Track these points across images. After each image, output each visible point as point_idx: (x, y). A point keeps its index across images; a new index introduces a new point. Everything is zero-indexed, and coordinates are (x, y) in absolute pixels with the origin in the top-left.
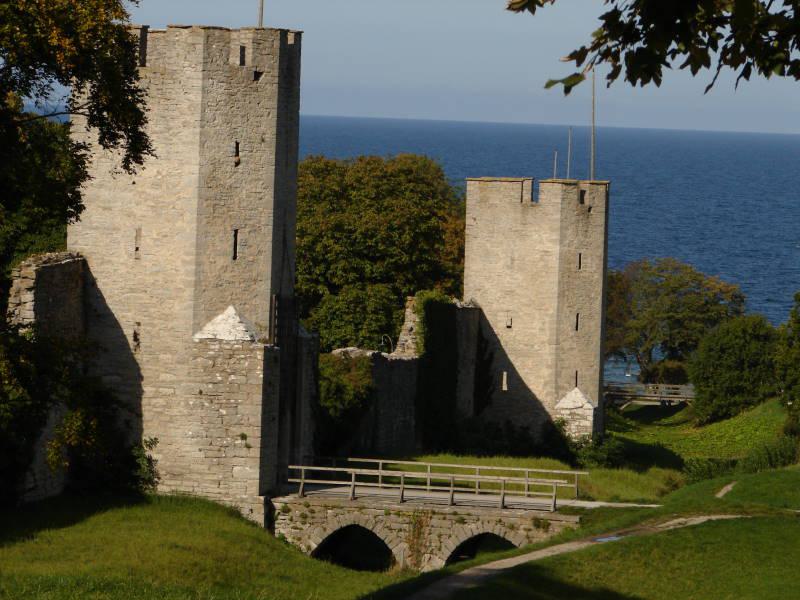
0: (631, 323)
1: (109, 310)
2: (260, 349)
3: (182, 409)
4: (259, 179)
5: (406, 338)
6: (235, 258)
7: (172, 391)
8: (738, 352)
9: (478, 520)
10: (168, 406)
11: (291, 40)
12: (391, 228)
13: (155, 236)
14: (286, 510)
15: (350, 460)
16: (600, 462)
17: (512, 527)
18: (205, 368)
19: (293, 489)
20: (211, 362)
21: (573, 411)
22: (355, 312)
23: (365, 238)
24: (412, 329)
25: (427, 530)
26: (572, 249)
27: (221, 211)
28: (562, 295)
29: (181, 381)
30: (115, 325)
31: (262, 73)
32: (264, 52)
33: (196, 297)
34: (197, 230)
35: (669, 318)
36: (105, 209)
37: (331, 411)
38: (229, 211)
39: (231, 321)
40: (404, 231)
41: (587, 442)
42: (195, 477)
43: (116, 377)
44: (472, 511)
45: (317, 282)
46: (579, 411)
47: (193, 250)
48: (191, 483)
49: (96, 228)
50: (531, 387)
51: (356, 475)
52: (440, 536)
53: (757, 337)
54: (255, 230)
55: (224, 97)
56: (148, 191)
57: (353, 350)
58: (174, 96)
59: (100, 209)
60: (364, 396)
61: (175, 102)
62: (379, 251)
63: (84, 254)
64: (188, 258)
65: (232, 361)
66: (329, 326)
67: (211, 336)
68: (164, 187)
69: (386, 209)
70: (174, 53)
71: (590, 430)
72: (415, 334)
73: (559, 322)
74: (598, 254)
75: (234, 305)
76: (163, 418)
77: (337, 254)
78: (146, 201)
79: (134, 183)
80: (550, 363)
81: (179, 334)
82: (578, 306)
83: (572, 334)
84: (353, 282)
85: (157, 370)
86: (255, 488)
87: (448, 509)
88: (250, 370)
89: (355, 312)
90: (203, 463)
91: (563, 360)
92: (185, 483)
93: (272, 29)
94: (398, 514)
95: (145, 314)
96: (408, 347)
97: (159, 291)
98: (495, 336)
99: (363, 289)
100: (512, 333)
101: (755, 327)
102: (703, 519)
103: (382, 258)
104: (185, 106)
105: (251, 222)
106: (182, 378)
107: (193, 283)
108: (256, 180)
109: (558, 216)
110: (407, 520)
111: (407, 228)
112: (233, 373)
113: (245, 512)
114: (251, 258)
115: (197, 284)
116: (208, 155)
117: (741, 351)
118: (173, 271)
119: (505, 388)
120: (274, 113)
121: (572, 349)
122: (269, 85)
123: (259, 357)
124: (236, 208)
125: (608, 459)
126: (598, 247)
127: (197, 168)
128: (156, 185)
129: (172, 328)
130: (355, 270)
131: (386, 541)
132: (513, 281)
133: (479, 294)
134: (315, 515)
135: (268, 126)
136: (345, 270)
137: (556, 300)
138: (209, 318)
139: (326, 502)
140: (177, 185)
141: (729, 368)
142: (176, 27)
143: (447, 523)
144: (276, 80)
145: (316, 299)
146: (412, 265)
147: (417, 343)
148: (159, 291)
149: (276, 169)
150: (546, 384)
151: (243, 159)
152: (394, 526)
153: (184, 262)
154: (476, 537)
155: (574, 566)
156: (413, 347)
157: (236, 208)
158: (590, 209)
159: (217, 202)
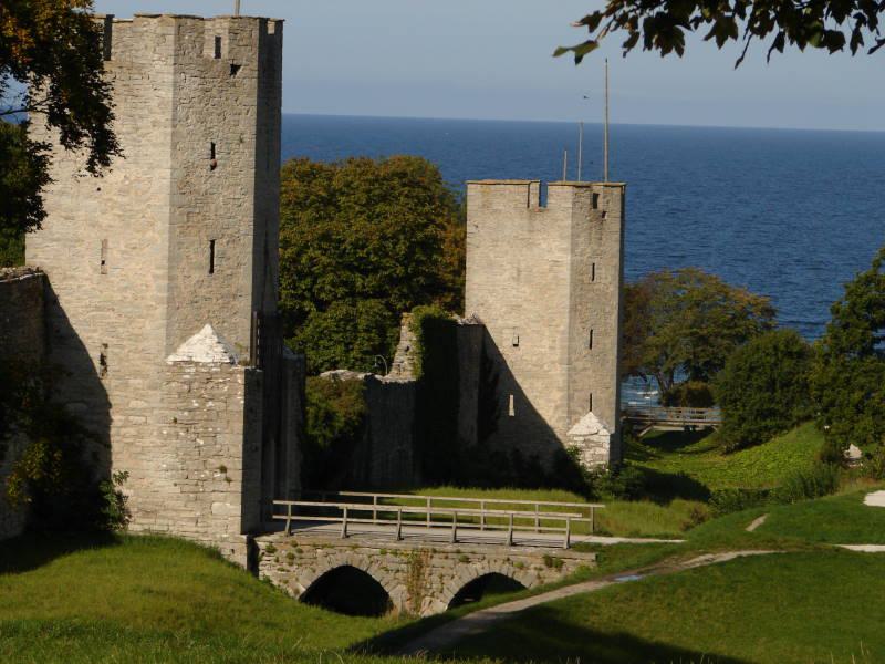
0: (651, 339)
2: (240, 372)
6: (212, 271)
7: (143, 419)
8: (768, 371)
9: (484, 558)
10: (139, 436)
11: (271, 30)
12: (384, 238)
13: (123, 248)
14: (271, 550)
15: (341, 493)
16: (618, 494)
17: (522, 567)
18: (180, 394)
19: (278, 526)
20: (186, 387)
22: (345, 331)
24: (408, 349)
28: (573, 309)
30: (80, 347)
31: (239, 67)
32: (241, 43)
33: (169, 316)
35: (692, 334)
36: (67, 218)
39: (208, 341)
40: (399, 240)
41: (603, 472)
42: (170, 514)
43: (80, 405)
44: (477, 549)
45: (303, 298)
46: (595, 438)
47: (165, 263)
48: (166, 522)
49: (58, 240)
50: (540, 412)
51: (349, 511)
52: (441, 577)
53: (790, 354)
54: (233, 240)
55: (199, 94)
56: (115, 198)
57: (343, 373)
58: (142, 92)
61: (143, 99)
62: (372, 262)
63: (45, 269)
64: (159, 272)
65: (210, 386)
66: (316, 347)
67: (185, 359)
68: (132, 195)
71: (605, 461)
72: (412, 354)
73: (571, 339)
74: (614, 264)
75: (211, 323)
76: (134, 449)
77: (325, 267)
78: (112, 209)
79: (99, 189)
80: (561, 386)
84: (343, 297)
85: (126, 397)
86: (236, 526)
87: (450, 548)
90: (178, 498)
91: (575, 382)
92: (160, 521)
93: (250, 17)
94: (395, 554)
96: (404, 368)
98: (500, 355)
99: (354, 305)
101: (787, 344)
102: (731, 555)
103: (375, 270)
104: (154, 103)
105: (229, 232)
107: (165, 300)
109: (569, 222)
110: (405, 559)
111: (402, 237)
113: (226, 553)
114: (229, 272)
115: (170, 300)
116: (181, 158)
117: (772, 370)
118: (144, 287)
119: (512, 413)
120: (254, 110)
122: (248, 79)
123: (240, 381)
125: (627, 491)
128: (123, 192)
130: (345, 284)
132: (520, 294)
133: (482, 309)
134: (303, 555)
135: (247, 125)
136: (333, 284)
137: (567, 315)
138: (184, 339)
140: (146, 192)
141: (760, 388)
143: (450, 562)
145: (301, 317)
146: (407, 278)
148: (129, 309)
149: (256, 173)
150: (557, 408)
152: (390, 566)
156: (410, 368)
158: (604, 213)
159: (190, 210)
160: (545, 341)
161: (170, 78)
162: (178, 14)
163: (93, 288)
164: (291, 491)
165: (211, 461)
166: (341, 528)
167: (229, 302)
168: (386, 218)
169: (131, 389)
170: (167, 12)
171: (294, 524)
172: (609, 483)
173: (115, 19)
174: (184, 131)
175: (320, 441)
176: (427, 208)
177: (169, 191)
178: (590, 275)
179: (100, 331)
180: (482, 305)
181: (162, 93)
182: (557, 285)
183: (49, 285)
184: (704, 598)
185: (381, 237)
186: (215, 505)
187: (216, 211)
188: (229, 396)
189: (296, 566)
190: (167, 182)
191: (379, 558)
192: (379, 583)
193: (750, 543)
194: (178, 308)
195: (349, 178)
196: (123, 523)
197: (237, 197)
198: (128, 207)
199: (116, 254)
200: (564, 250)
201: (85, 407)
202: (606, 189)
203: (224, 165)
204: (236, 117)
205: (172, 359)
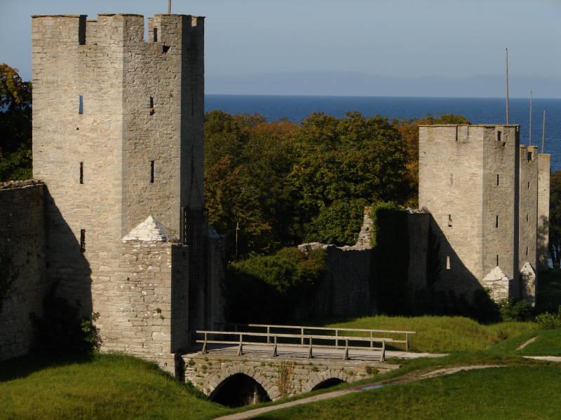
1: (64, 221)
2: (168, 247)
3: (115, 292)
4: (169, 124)
5: (364, 235)
6: (152, 181)
7: (108, 278)
9: (327, 369)
10: (105, 289)
11: (194, 23)
13: (94, 167)
14: (192, 363)
15: (250, 325)
16: (513, 317)
17: (352, 374)
18: (131, 262)
20: (135, 257)
21: (496, 282)
22: (342, 218)
23: (349, 168)
24: (368, 229)
25: (291, 376)
26: (492, 172)
27: (140, 147)
28: (485, 203)
29: (114, 271)
30: (68, 231)
33: (124, 211)
34: (123, 162)
36: (58, 148)
37: (279, 288)
38: (146, 148)
39: (149, 227)
40: (376, 162)
41: (505, 304)
42: (126, 340)
44: (323, 362)
45: (318, 198)
46: (500, 283)
47: (120, 176)
48: (122, 345)
49: (53, 162)
51: (305, 330)
52: (300, 381)
54: (167, 161)
55: (140, 65)
56: (88, 134)
58: (104, 65)
59: (55, 149)
60: (316, 277)
61: (104, 69)
62: (359, 176)
63: (45, 181)
64: (116, 182)
65: (149, 256)
66: (324, 228)
67: (134, 238)
68: (99, 131)
69: (364, 147)
70: (103, 34)
71: (506, 296)
72: (370, 232)
73: (484, 222)
75: (153, 216)
76: (102, 298)
78: (86, 142)
79: (78, 129)
80: (478, 250)
81: (112, 237)
82: (498, 210)
83: (493, 230)
87: (305, 361)
88: (162, 262)
89: (342, 218)
90: (131, 330)
91: (487, 248)
92: (119, 345)
93: (175, 15)
94: (271, 365)
95: (89, 223)
96: (365, 241)
97: (97, 207)
98: (441, 232)
100: (452, 230)
102: (456, 370)
103: (363, 180)
104: (111, 72)
105: (164, 155)
106: (115, 269)
107: (121, 200)
108: (166, 125)
109: (482, 149)
110: (277, 369)
112: (151, 265)
113: (161, 365)
114: (164, 181)
115: (124, 200)
116: (129, 108)
118: (107, 192)
119: (448, 267)
120: (179, 76)
121: (494, 240)
122: (175, 56)
123: (168, 253)
124: (152, 145)
125: (520, 315)
126: (510, 170)
127: (121, 117)
129: (107, 233)
131: (263, 385)
133: (429, 203)
134: (212, 366)
137: (481, 207)
138: (134, 226)
139: (220, 357)
140: (108, 130)
142: (104, 15)
143: (305, 371)
144: (180, 52)
145: (315, 211)
146: (383, 185)
147: (371, 239)
148: (97, 207)
150: (476, 264)
151: (156, 110)
152: (268, 374)
153: (114, 185)
154: (326, 381)
155: (311, 412)
156: (369, 241)
157: (152, 145)
158: (504, 143)
159: (137, 141)
160: (468, 223)
161: (121, 55)
162: (126, 13)
163: (75, 194)
164: (215, 324)
165: (151, 305)
166: (239, 348)
167: (164, 202)
168: (368, 148)
169: (100, 259)
170: (119, 13)
171: (209, 347)
172: (508, 310)
173: (88, 19)
174: (131, 90)
175: (279, 288)
176: (396, 142)
177: (122, 129)
178: (496, 182)
179: (80, 221)
180: (429, 201)
181: (116, 65)
182: (475, 188)
183: (48, 191)
184: (421, 401)
185: (365, 161)
186: (154, 334)
187: (155, 141)
188: (162, 262)
189: (207, 374)
190: (120, 123)
191: (261, 368)
192: (260, 385)
193: (480, 360)
194: (130, 206)
195: (347, 125)
196: (97, 346)
197: (168, 132)
198: (97, 140)
199: (91, 172)
200: (479, 167)
201: (72, 270)
202: (507, 129)
203: (159, 112)
204: (168, 80)
205: (126, 238)
